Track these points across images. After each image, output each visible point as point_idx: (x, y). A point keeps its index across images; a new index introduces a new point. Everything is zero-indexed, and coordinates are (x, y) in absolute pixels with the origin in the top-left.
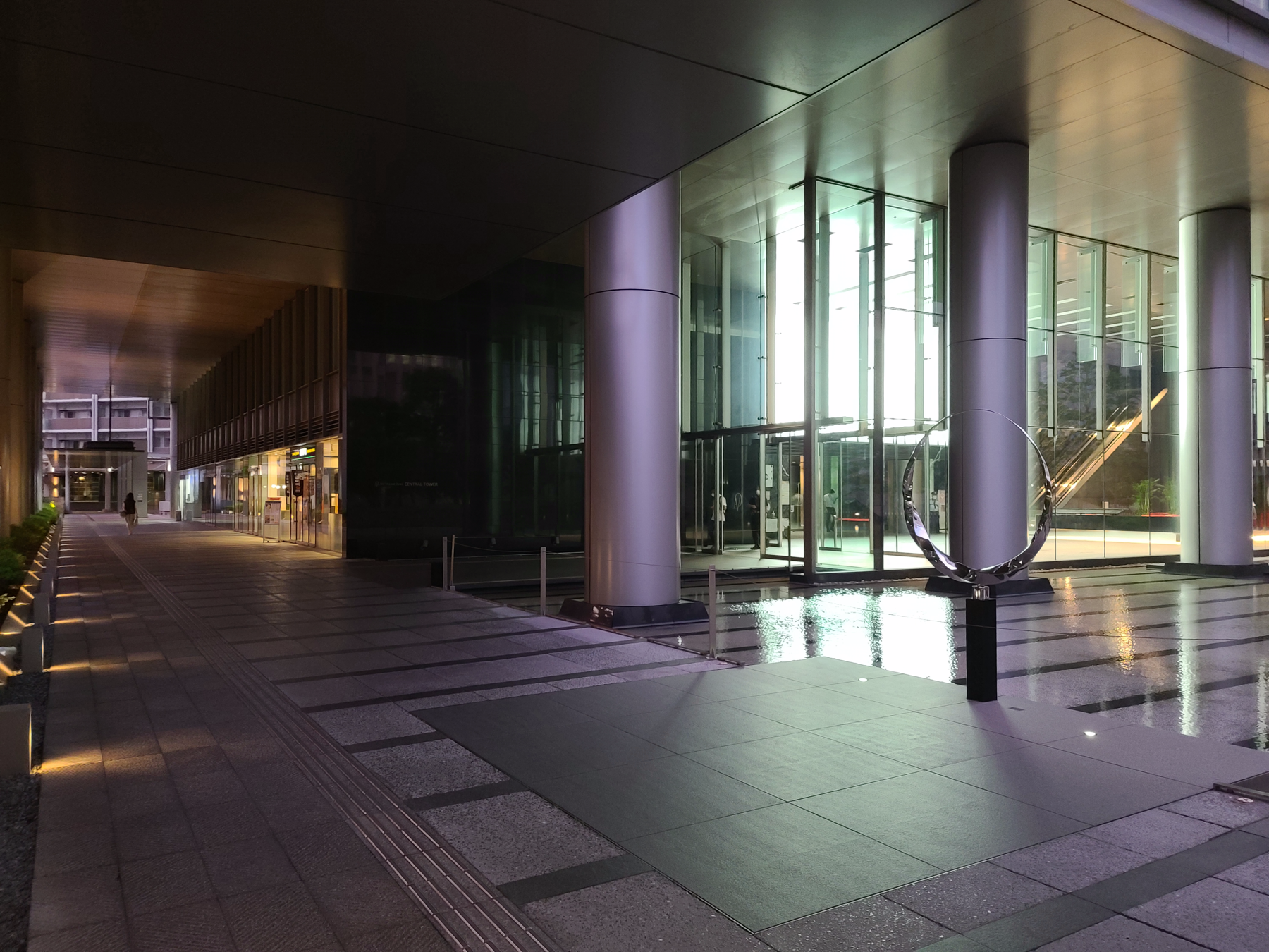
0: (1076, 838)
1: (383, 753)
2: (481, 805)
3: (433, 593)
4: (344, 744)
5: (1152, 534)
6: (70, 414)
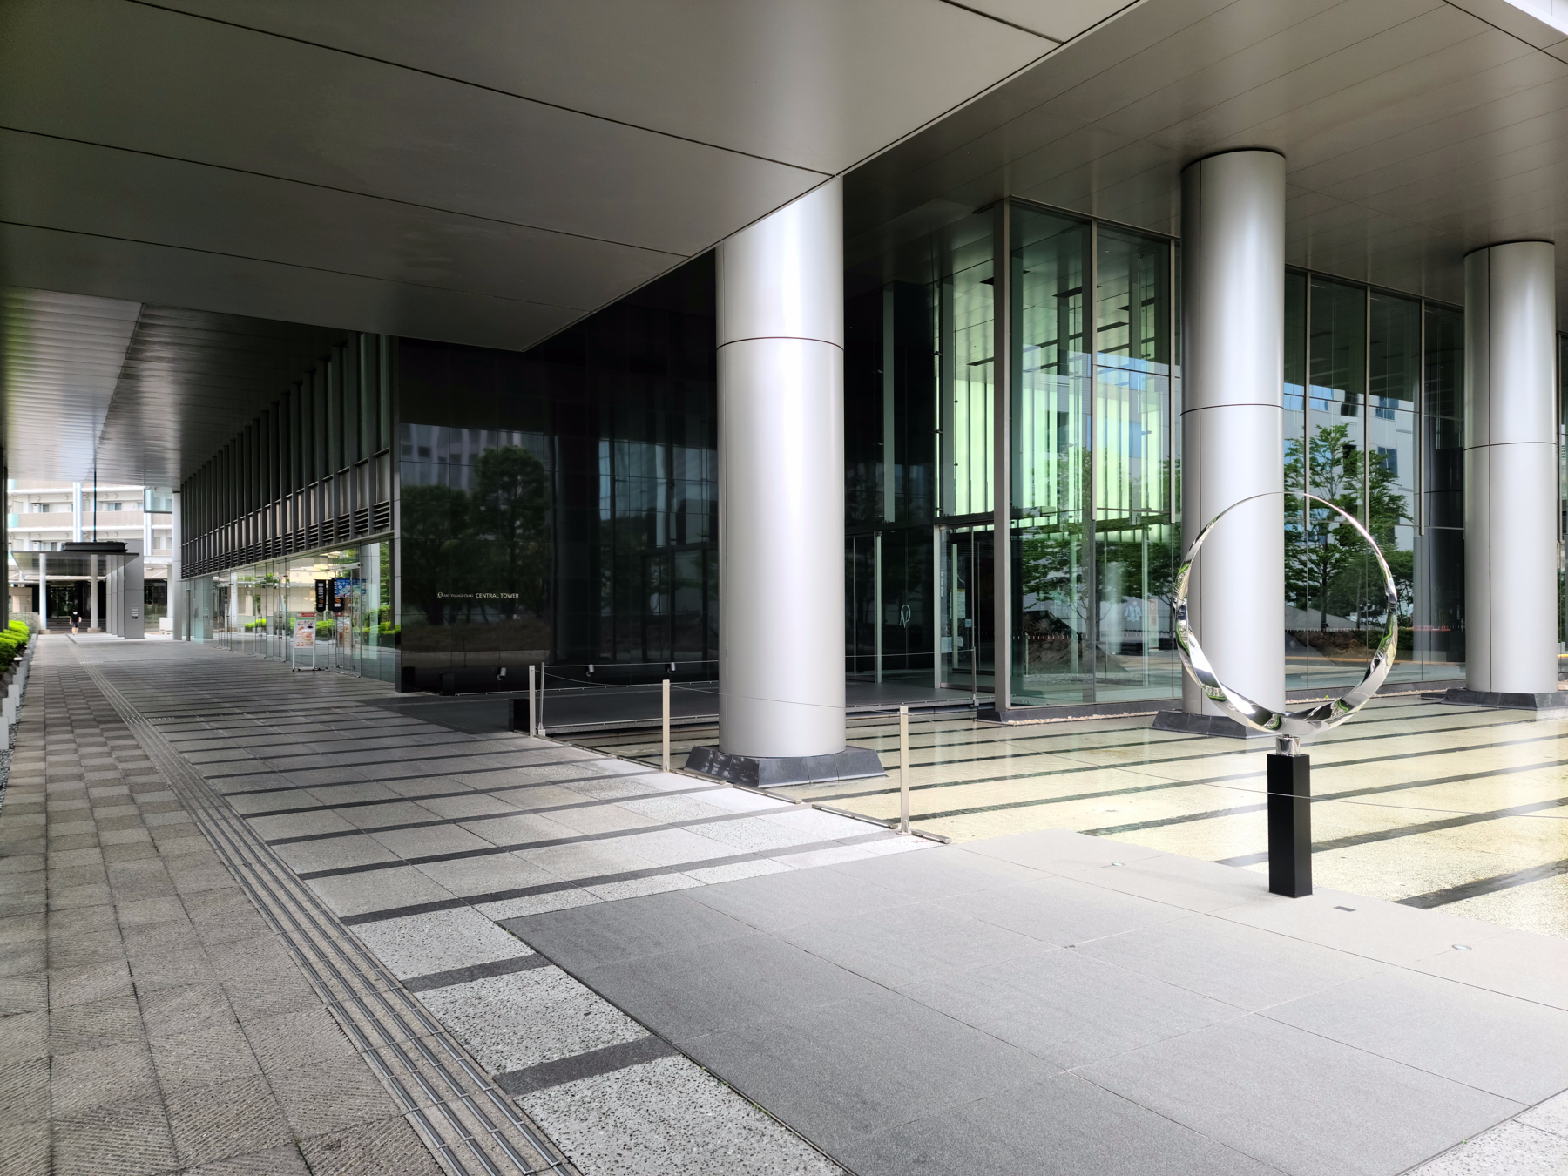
0: (1511, 1127)
1: (462, 991)
2: (610, 1082)
3: (514, 739)
4: (401, 977)
5: (1265, 778)
6: (45, 507)
